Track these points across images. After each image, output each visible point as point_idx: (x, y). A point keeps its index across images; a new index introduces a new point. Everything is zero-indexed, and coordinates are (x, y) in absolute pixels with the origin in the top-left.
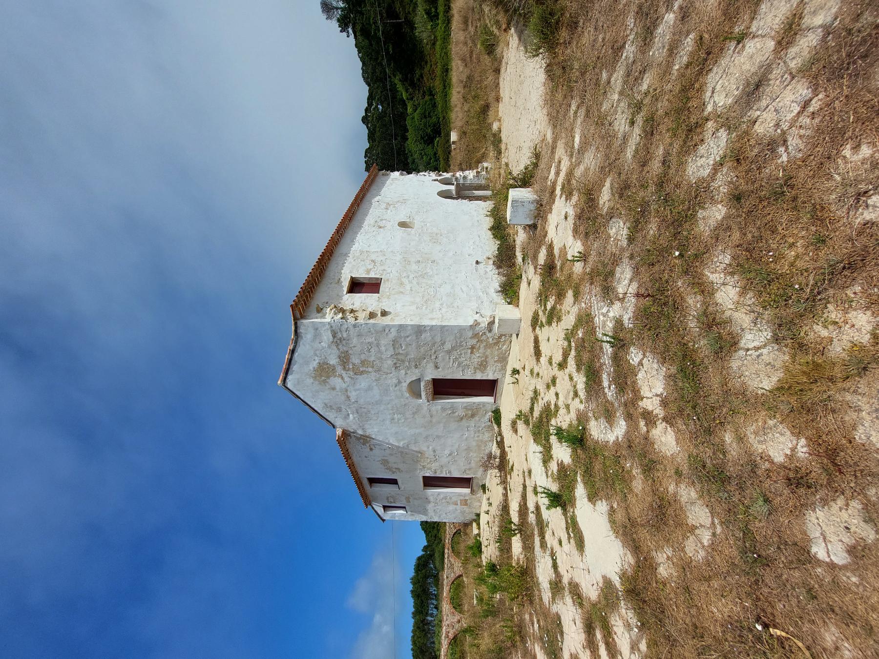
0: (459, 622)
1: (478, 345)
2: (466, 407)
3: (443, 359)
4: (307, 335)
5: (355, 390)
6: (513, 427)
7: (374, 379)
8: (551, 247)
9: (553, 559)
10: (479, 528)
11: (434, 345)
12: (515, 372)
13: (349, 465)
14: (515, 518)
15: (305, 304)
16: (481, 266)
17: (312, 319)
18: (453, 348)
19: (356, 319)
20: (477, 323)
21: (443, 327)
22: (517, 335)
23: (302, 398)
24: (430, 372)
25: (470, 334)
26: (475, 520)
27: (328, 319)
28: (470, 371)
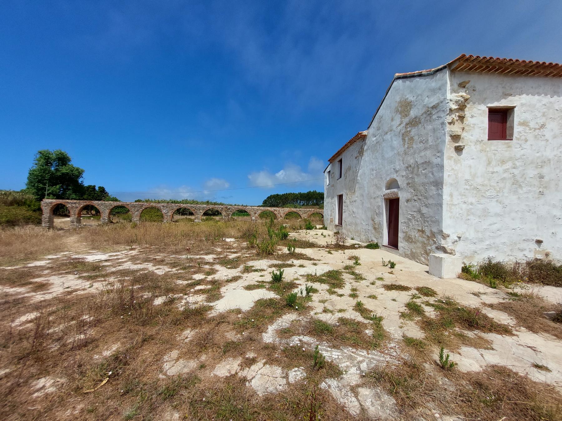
0: (281, 216)
1: (425, 236)
2: (380, 224)
3: (414, 206)
4: (433, 83)
5: (391, 138)
6: (353, 257)
7: (399, 150)
8: (505, 330)
9: (259, 270)
10: (319, 229)
11: (426, 198)
12: (393, 265)
13: (347, 145)
14: (298, 250)
15: (470, 69)
16: (535, 246)
17: (451, 81)
18: (422, 215)
19: (450, 123)
20: (445, 237)
21: (441, 205)
22: (427, 272)
23: (386, 97)
24: (404, 196)
25: (435, 230)
26: (324, 227)
27: (450, 96)
28: (404, 229)
